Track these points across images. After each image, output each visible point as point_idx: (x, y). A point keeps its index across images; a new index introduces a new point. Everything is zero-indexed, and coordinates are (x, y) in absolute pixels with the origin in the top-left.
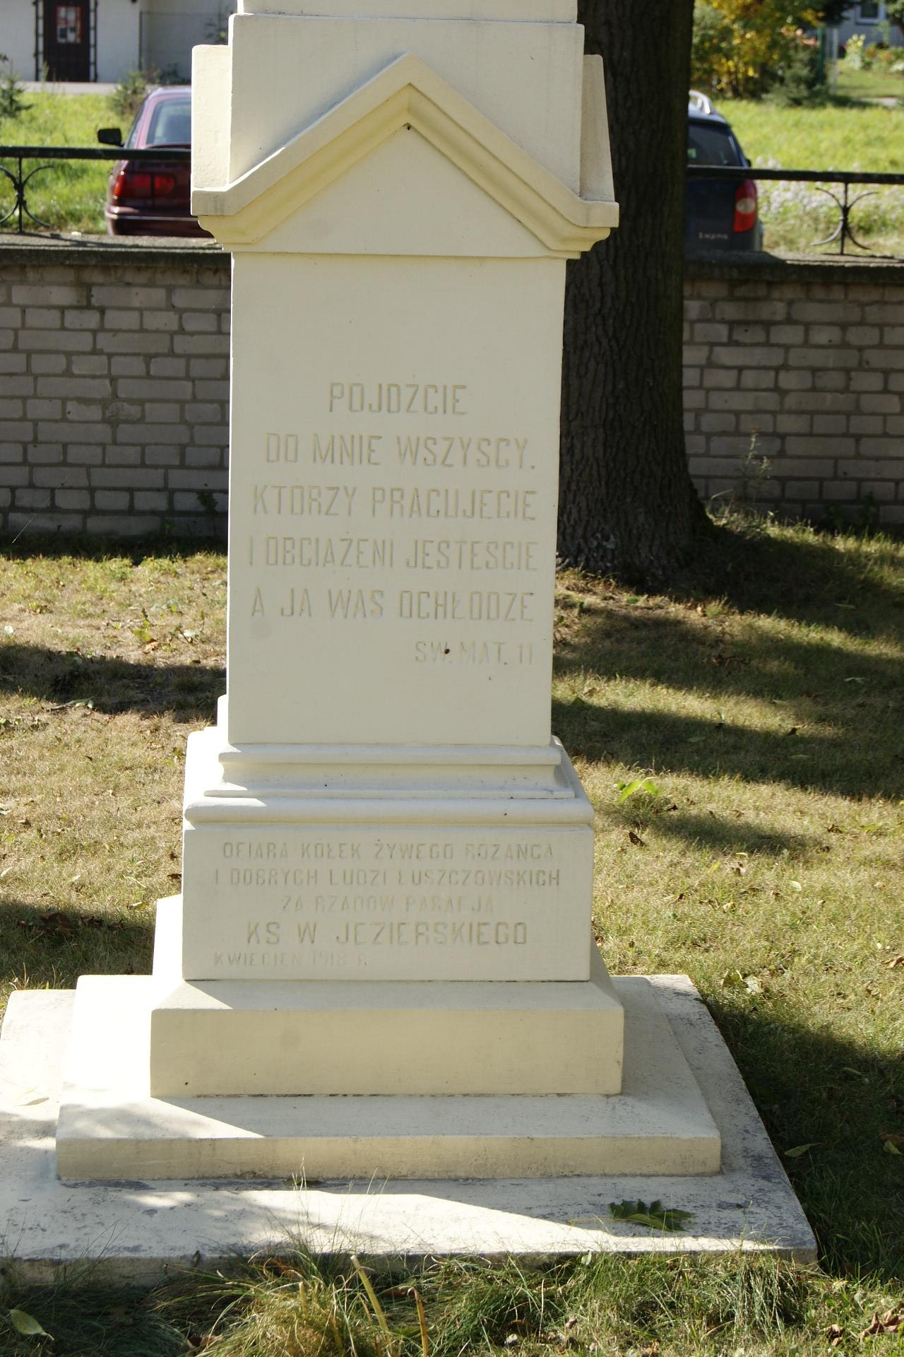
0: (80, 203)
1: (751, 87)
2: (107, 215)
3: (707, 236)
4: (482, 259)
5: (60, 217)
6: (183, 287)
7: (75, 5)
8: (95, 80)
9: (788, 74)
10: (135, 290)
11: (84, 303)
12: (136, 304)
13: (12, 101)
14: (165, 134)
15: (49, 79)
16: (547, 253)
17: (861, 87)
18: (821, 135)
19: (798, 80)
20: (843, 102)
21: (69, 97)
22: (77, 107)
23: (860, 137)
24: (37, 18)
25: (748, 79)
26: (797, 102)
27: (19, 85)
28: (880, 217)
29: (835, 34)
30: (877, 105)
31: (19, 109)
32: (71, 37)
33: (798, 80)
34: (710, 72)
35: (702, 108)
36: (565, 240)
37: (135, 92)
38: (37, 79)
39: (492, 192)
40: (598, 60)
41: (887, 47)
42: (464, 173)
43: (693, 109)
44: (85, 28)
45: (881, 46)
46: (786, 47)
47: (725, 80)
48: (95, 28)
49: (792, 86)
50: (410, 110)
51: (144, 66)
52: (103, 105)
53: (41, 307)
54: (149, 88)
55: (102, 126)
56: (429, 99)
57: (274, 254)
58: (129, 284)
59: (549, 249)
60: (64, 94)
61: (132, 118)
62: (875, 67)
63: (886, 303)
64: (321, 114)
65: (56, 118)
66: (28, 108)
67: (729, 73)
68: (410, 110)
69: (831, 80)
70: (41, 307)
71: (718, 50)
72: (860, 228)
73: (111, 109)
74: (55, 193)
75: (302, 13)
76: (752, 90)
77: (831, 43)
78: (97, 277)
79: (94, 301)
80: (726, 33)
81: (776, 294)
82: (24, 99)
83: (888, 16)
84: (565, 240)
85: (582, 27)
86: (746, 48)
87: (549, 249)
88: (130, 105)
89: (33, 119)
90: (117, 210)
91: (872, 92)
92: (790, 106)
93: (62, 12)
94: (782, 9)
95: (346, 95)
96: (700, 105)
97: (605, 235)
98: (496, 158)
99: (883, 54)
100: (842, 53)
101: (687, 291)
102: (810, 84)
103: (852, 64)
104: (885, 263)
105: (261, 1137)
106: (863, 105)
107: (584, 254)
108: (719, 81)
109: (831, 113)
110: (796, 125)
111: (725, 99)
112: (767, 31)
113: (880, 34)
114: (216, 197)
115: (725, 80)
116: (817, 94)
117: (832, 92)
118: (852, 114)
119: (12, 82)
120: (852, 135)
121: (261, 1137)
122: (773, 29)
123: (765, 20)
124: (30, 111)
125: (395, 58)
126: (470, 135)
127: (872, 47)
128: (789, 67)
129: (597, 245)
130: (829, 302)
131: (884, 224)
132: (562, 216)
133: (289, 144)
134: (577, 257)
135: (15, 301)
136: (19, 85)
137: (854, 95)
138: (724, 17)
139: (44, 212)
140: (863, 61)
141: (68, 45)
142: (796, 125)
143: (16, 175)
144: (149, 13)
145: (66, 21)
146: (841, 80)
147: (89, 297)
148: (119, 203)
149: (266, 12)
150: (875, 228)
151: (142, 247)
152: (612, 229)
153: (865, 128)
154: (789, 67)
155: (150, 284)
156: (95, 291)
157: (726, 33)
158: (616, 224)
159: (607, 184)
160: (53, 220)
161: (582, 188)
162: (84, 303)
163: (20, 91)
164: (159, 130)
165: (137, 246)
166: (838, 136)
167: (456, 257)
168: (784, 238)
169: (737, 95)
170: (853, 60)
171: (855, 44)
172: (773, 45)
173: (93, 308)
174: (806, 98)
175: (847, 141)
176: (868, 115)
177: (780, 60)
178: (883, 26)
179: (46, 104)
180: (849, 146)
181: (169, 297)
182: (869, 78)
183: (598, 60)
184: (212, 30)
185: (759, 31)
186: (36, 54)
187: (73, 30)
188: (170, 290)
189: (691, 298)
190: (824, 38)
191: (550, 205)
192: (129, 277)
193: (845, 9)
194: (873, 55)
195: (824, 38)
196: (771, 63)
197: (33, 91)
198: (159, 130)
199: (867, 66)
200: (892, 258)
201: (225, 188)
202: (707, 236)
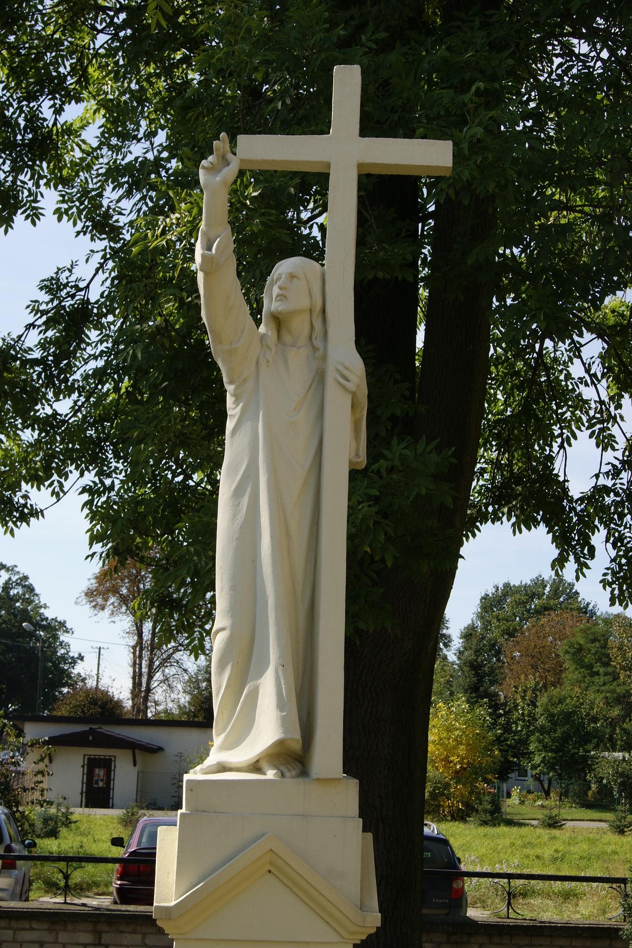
0: (100, 877)
1: (460, 814)
2: (114, 885)
3: (437, 901)
4: (308, 943)
5: (89, 885)
6: (151, 933)
7: (104, 767)
8: (112, 808)
9: (480, 808)
10: (125, 935)
11: (97, 942)
12: (125, 943)
13: (67, 818)
14: (147, 841)
15: (87, 806)
16: (342, 940)
17: (519, 814)
18: (499, 841)
19: (485, 811)
20: (510, 823)
21: (98, 817)
22: (102, 822)
23: (519, 842)
24: (83, 774)
25: (459, 810)
26: (485, 823)
27: (72, 810)
28: (531, 888)
29: (505, 787)
30: (528, 825)
31: (70, 823)
32: (101, 784)
33: (485, 811)
34: (439, 806)
35: (433, 831)
36: (352, 933)
37: (133, 815)
38: (81, 807)
39: (314, 907)
40: (370, 836)
41: (533, 792)
42: (299, 897)
43: (426, 830)
44: (108, 779)
45: (529, 792)
46: (479, 793)
47: (447, 810)
48: (114, 780)
49: (483, 815)
50: (271, 863)
51: (138, 800)
52: (115, 821)
53: (74, 944)
54: (141, 812)
55: (115, 836)
56: (281, 858)
57: (197, 939)
58: (122, 932)
59: (344, 938)
60: (95, 815)
61: (131, 829)
62: (526, 803)
63: (533, 945)
64: (224, 865)
65: (90, 828)
66: (75, 822)
67: (449, 807)
68: (271, 863)
69: (503, 810)
70: (74, 944)
71: (443, 794)
72: (521, 894)
73: (119, 823)
74: (87, 871)
75: (215, 812)
76: (460, 816)
77: (503, 791)
78: (105, 928)
79: (102, 941)
80: (447, 786)
81: (473, 940)
82: (73, 818)
83: (532, 776)
84: (352, 933)
85: (361, 820)
86: (458, 793)
87: (344, 938)
88: (129, 822)
89: (78, 828)
90: (119, 882)
91: (526, 817)
92: (481, 825)
93: (97, 771)
94: (476, 773)
95: (237, 855)
96: (432, 828)
97: (374, 931)
98: (315, 889)
99: (530, 796)
100: (509, 795)
101: (424, 938)
102: (492, 813)
103: (514, 801)
104: (532, 923)
105: (437, 441)
106: (520, 825)
107: (362, 940)
108: (444, 811)
109: (503, 829)
110: (485, 836)
111: (447, 820)
112: (468, 785)
113: (529, 786)
114: (167, 909)
115: (447, 810)
116: (496, 819)
117: (504, 817)
118: (515, 830)
119: (68, 808)
120: (515, 841)
121: (437, 441)
122: (472, 784)
123: (467, 779)
124: (77, 824)
125: (263, 835)
126: (302, 877)
127: (524, 792)
128: (481, 804)
129: (370, 936)
130: (502, 944)
131: (533, 892)
132: (351, 920)
133: (206, 881)
134: (359, 942)
135: (60, 940)
136: (72, 810)
137: (516, 818)
138: (446, 777)
139: (80, 882)
140: (520, 800)
141: (99, 788)
142: (485, 836)
143: (65, 871)
144: (142, 772)
145: (99, 776)
146: (508, 810)
147: (100, 938)
148: (119, 879)
149: (197, 811)
150: (529, 894)
151: (130, 911)
152: (377, 928)
153: (522, 837)
154: (481, 804)
155: (134, 932)
156: (103, 935)
157: (447, 786)
158: (379, 925)
159: (375, 903)
160: (85, 886)
161: (361, 905)
162: (97, 942)
163: (72, 813)
164: (144, 840)
165: (128, 911)
166: (507, 842)
167: (293, 942)
168: (480, 899)
169: (454, 819)
170: (515, 800)
171: (516, 792)
172: (471, 793)
173: (102, 945)
174: (490, 821)
175: (513, 844)
176: (524, 830)
177: (476, 800)
178: (530, 782)
179: (85, 820)
180: (514, 848)
181: (143, 939)
182: (524, 809)
183: (370, 836)
184: (175, 781)
185: (464, 785)
186: (82, 793)
187: (102, 780)
188: (144, 935)
189: (427, 942)
190: (499, 788)
191: (344, 914)
192: (122, 928)
193: (510, 773)
194: (525, 797)
195: (499, 788)
196: (471, 802)
197: (79, 813)
198: (144, 840)
199: (522, 803)
200: (535, 920)
201: (173, 903)
202: (437, 901)
